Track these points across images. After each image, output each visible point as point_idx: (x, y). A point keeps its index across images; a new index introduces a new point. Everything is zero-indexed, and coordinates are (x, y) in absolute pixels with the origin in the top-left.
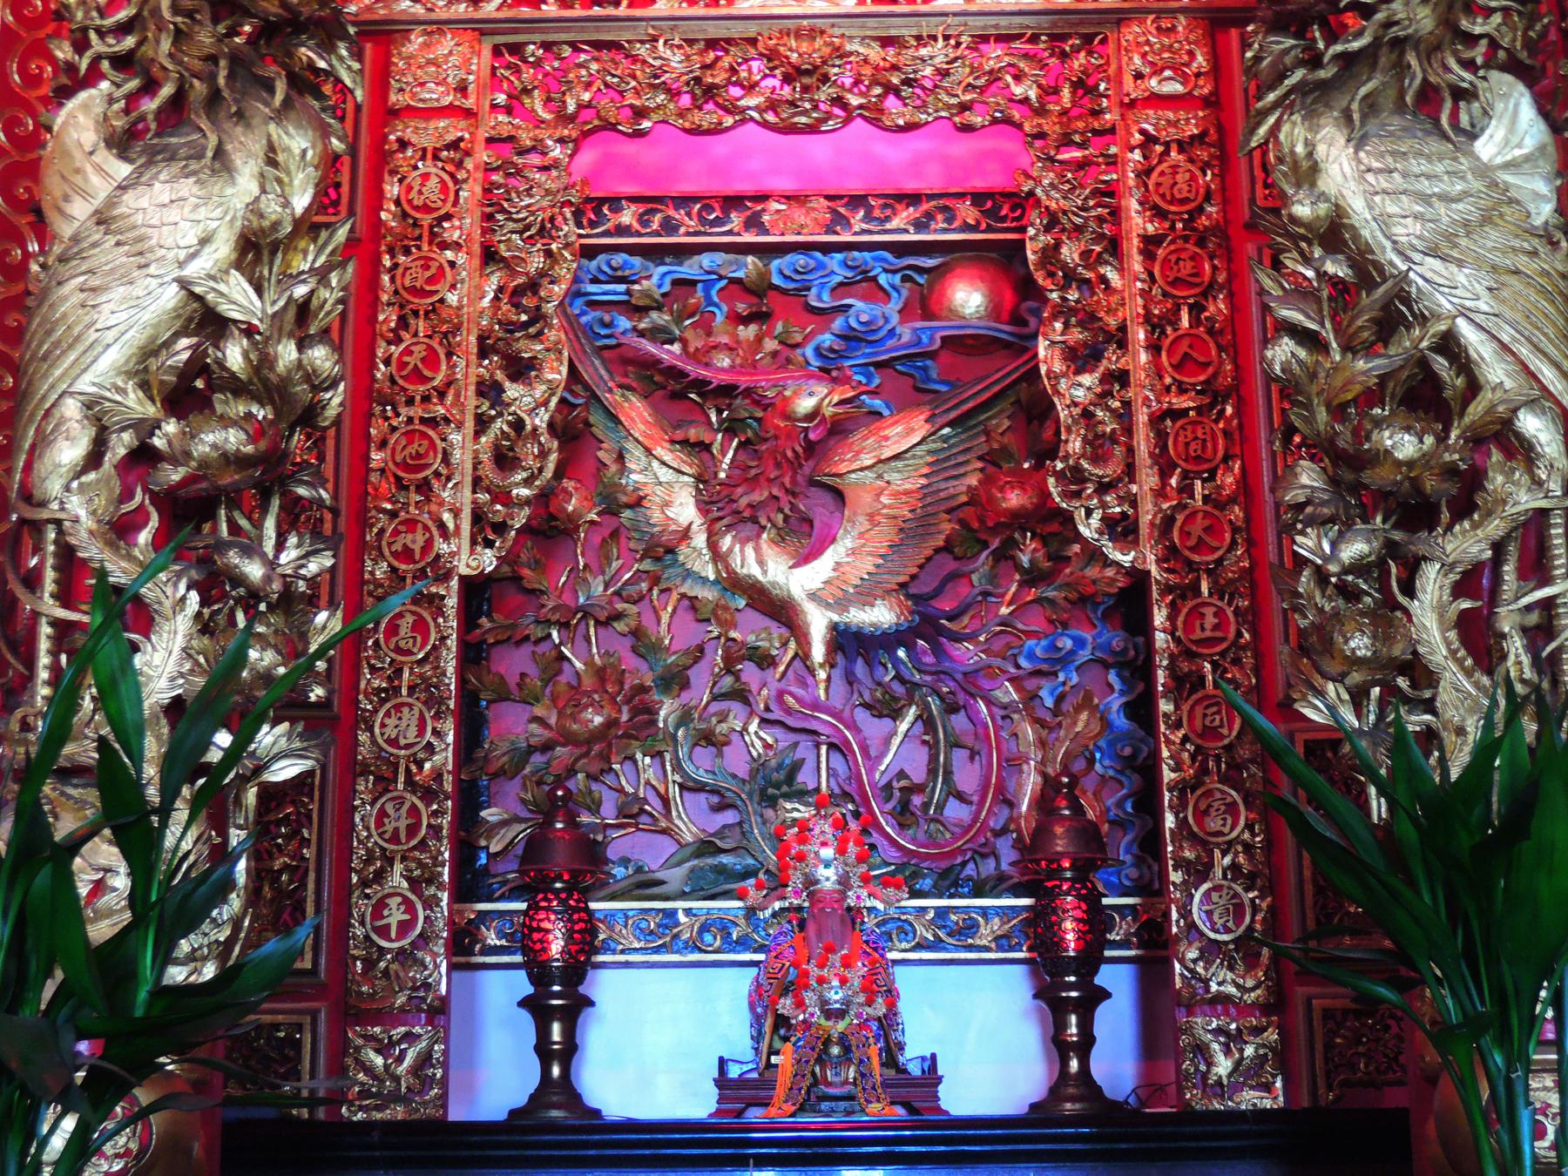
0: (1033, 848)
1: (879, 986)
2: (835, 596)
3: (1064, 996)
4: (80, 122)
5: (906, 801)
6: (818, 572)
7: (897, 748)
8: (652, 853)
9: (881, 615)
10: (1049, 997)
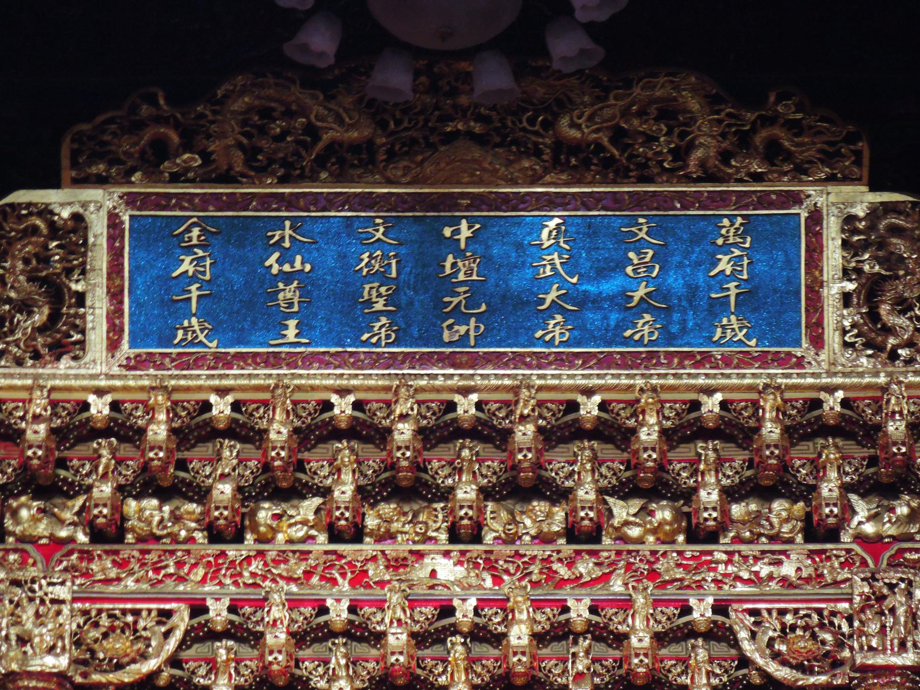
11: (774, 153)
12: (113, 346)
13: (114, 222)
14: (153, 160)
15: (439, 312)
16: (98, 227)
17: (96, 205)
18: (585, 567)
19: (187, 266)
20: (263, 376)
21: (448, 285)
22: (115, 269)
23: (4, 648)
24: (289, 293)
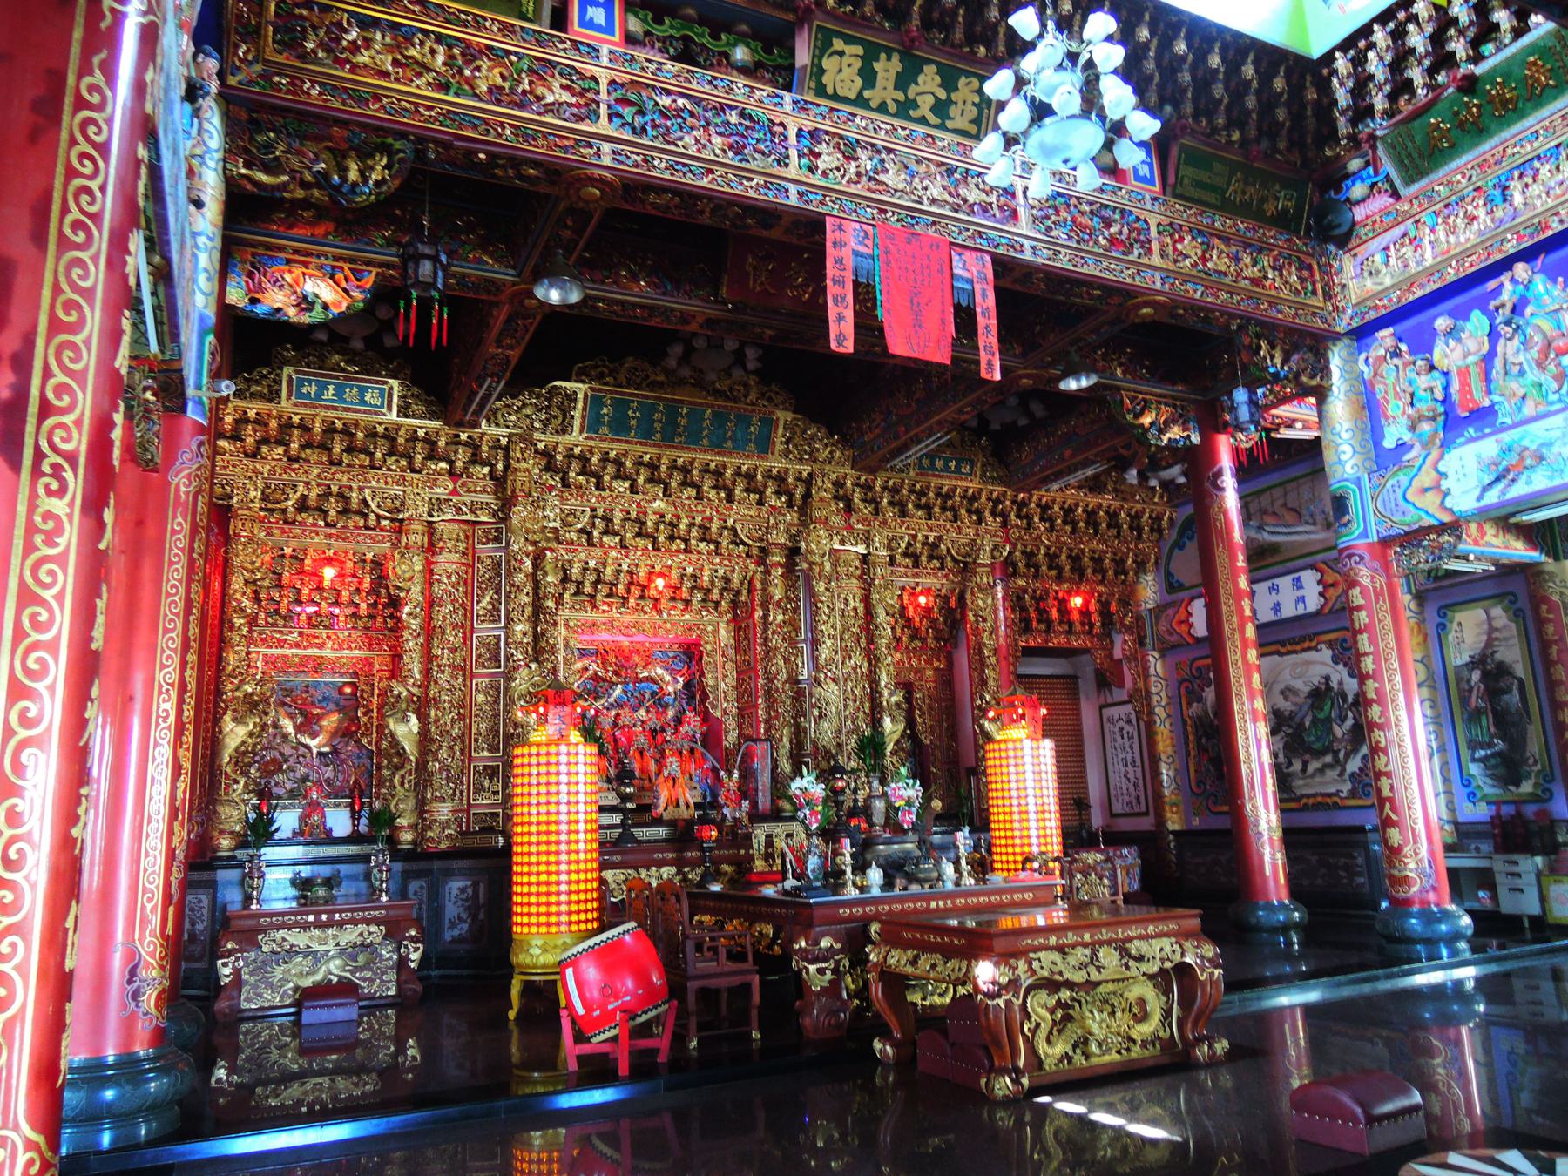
0: (352, 791)
1: (323, 816)
2: (320, 746)
3: (355, 817)
4: (227, 718)
5: (329, 782)
6: (316, 741)
7: (329, 773)
8: (281, 792)
9: (326, 749)
10: (353, 817)
11: (770, 400)
12: (581, 432)
13: (586, 395)
14: (600, 378)
15: (674, 433)
16: (580, 396)
17: (580, 388)
18: (700, 508)
19: (605, 410)
20: (626, 446)
21: (678, 426)
22: (584, 409)
23: (690, 11)
24: (633, 422)
